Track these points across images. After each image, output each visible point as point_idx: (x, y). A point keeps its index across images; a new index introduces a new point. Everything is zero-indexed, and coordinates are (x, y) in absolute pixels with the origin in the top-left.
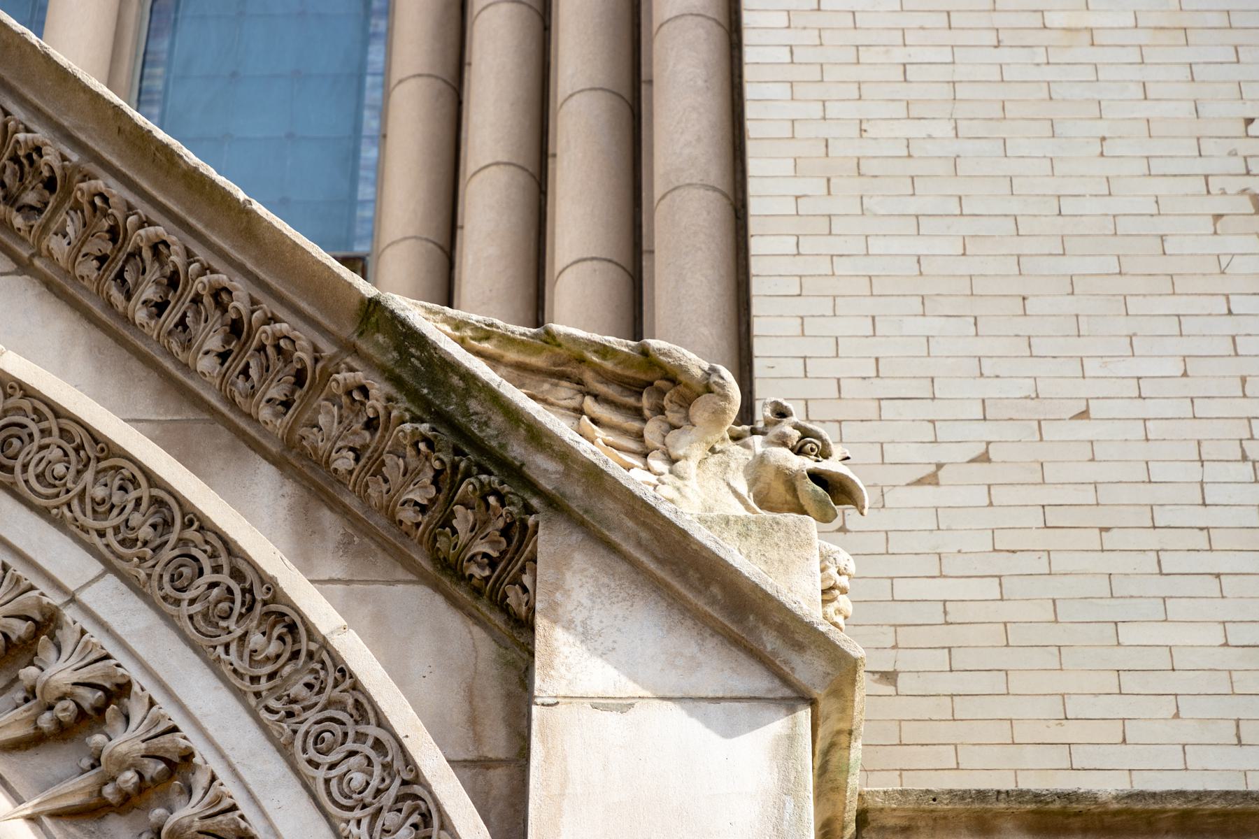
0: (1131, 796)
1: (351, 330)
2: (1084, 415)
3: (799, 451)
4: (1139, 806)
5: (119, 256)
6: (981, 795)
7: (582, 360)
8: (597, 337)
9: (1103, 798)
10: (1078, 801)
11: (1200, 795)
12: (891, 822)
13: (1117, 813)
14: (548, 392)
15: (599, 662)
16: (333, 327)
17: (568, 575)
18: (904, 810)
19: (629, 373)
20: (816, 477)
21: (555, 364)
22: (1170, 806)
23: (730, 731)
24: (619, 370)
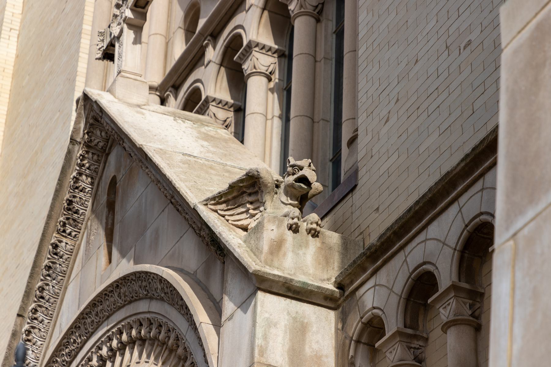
2: (417, 61)
4: (383, 240)
13: (382, 244)
19: (250, 182)
24: (247, 183)
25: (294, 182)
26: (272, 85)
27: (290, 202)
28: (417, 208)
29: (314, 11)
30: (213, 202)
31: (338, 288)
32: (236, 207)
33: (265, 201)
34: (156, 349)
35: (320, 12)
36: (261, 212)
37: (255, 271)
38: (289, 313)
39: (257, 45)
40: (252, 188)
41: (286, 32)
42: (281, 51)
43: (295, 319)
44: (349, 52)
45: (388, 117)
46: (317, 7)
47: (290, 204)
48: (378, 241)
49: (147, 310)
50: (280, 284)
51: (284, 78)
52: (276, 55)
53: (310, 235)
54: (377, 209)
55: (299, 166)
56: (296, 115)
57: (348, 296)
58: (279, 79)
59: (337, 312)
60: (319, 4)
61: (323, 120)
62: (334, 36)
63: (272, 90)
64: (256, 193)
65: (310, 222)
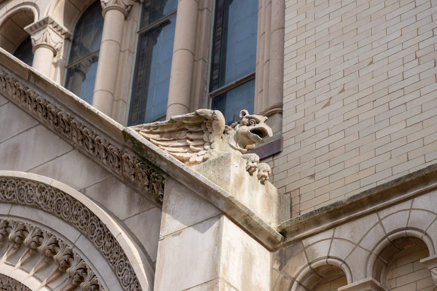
0: (351, 198)
1: (123, 141)
2: (372, 63)
3: (249, 125)
4: (354, 200)
5: (84, 139)
6: (311, 213)
7: (184, 123)
8: (184, 115)
9: (344, 202)
10: (338, 205)
11: (370, 190)
12: (293, 230)
13: (351, 204)
14: (178, 136)
15: (175, 221)
16: (120, 142)
17: (170, 196)
18: (293, 225)
19: (197, 122)
20: (254, 131)
21: (178, 127)
22: (363, 197)
23: (203, 231)
24: (193, 122)
25: (249, 132)
26: (55, 60)
27: (239, 148)
28: (407, 180)
29: (126, 8)
30: (146, 130)
31: (280, 233)
32: (170, 141)
33: (213, 142)
34: (10, 251)
35: (129, 12)
36: (205, 149)
37: (230, 197)
38: (242, 243)
39: (52, 23)
40: (196, 127)
41: (74, 21)
42: (69, 34)
43: (246, 249)
44: (181, 49)
45: (329, 102)
46: (127, 6)
47: (239, 150)
48: (348, 200)
49: (7, 214)
50: (243, 215)
51: (66, 57)
52: (63, 37)
53: (260, 181)
54: (313, 176)
55: (256, 119)
56: (102, 89)
57: (290, 243)
58: (63, 58)
59: (272, 253)
60: (130, 5)
61: (123, 100)
62: (138, 35)
63: (55, 65)
64: (202, 133)
65: (263, 169)
